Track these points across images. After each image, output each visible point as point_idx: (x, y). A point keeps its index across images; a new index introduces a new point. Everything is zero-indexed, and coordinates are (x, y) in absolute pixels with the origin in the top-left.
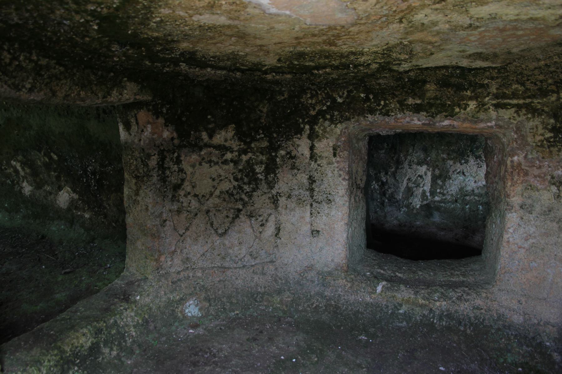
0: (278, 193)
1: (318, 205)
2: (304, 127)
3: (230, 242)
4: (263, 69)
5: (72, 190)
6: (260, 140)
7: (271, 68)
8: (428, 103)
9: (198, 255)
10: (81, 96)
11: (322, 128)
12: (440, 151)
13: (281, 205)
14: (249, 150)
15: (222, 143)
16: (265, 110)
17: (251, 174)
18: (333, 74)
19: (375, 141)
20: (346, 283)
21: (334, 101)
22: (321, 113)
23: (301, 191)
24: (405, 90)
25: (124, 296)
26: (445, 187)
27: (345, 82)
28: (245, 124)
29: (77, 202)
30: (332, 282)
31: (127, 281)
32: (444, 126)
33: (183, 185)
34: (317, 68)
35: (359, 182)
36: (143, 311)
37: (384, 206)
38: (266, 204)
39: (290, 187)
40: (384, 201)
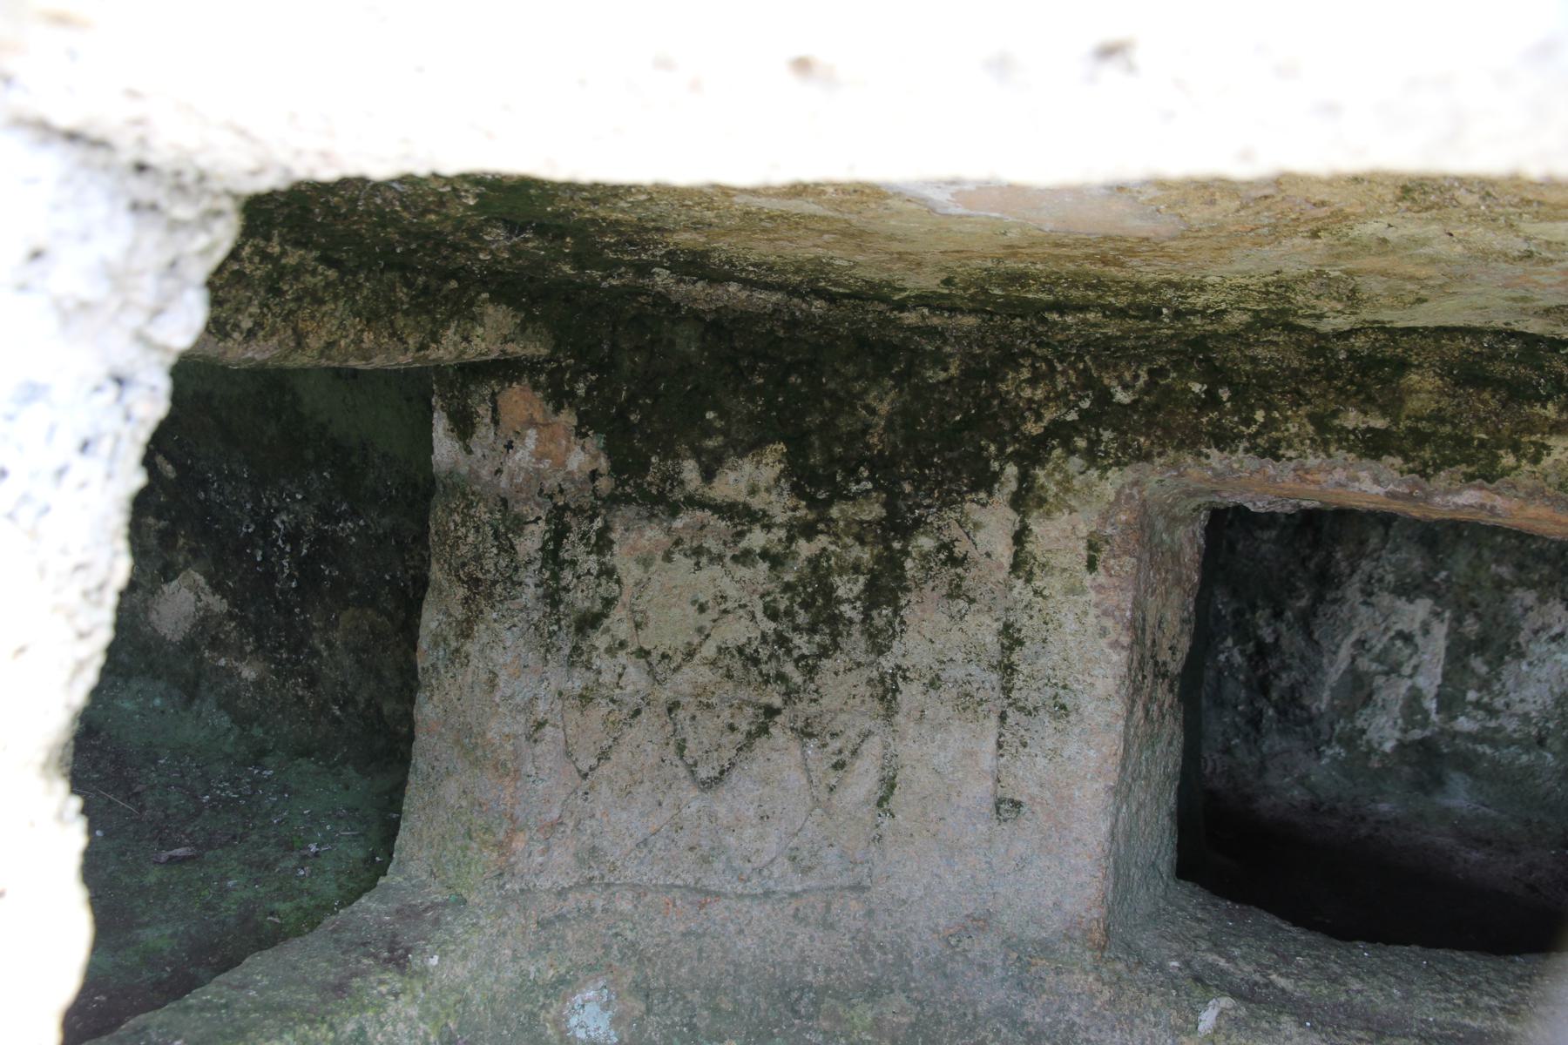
0: (899, 667)
1: (1021, 717)
2: (1002, 469)
3: (731, 809)
5: (209, 582)
7: (916, 297)
8: (1412, 431)
9: (630, 843)
11: (1058, 477)
12: (1486, 554)
13: (904, 708)
14: (821, 526)
15: (741, 499)
16: (884, 408)
18: (1106, 326)
19: (1227, 526)
20: (1097, 986)
21: (1104, 396)
22: (1061, 432)
23: (972, 668)
24: (1339, 383)
25: (392, 950)
26: (1497, 687)
28: (817, 443)
29: (220, 624)
30: (1051, 979)
31: (397, 905)
32: (1458, 508)
33: (607, 616)
34: (1061, 307)
35: (1164, 656)
36: (444, 1007)
37: (1258, 730)
38: (858, 700)
39: (941, 652)
40: (1261, 713)
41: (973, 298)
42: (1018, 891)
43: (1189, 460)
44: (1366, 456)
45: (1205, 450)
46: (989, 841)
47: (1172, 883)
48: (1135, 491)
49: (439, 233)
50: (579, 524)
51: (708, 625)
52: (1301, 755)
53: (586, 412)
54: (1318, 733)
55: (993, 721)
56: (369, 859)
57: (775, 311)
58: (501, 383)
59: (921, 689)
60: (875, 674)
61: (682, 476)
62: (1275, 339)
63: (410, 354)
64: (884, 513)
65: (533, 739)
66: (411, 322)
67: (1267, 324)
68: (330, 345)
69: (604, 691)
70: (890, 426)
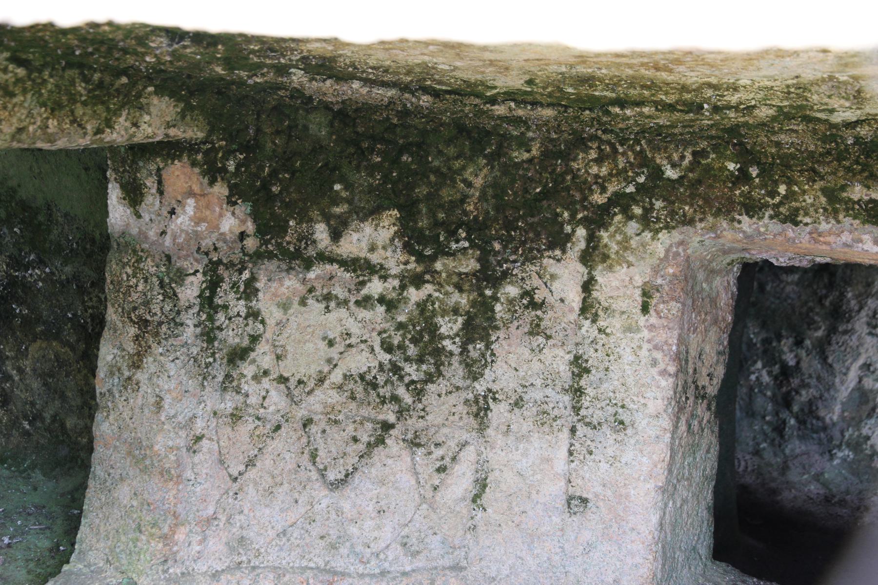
0: (490, 390)
2: (574, 231)
3: (354, 505)
4: (488, 94)
6: (459, 255)
9: (272, 533)
10: (49, 131)
11: (619, 237)
13: (494, 423)
14: (427, 277)
15: (362, 255)
16: (478, 182)
17: (426, 338)
18: (658, 118)
19: (755, 279)
21: (657, 173)
22: (621, 202)
23: (549, 391)
24: (847, 163)
27: (689, 133)
28: (424, 210)
33: (253, 350)
34: (622, 103)
35: (704, 381)
37: (782, 436)
38: (457, 417)
39: (524, 378)
40: (784, 422)
41: (550, 95)
42: (585, 570)
43: (725, 224)
44: (868, 222)
45: (737, 217)
46: (562, 530)
47: (709, 563)
48: (680, 250)
49: (112, 40)
50: (230, 276)
51: (336, 356)
52: (817, 457)
53: (236, 184)
54: (831, 439)
55: (565, 434)
56: (54, 549)
57: (390, 103)
58: (165, 161)
59: (508, 408)
60: (471, 396)
61: (315, 236)
62: (795, 128)
63: (88, 138)
64: (478, 267)
65: (192, 450)
66: (89, 111)
67: (789, 117)
68: (20, 130)
69: (251, 411)
70: (483, 197)
